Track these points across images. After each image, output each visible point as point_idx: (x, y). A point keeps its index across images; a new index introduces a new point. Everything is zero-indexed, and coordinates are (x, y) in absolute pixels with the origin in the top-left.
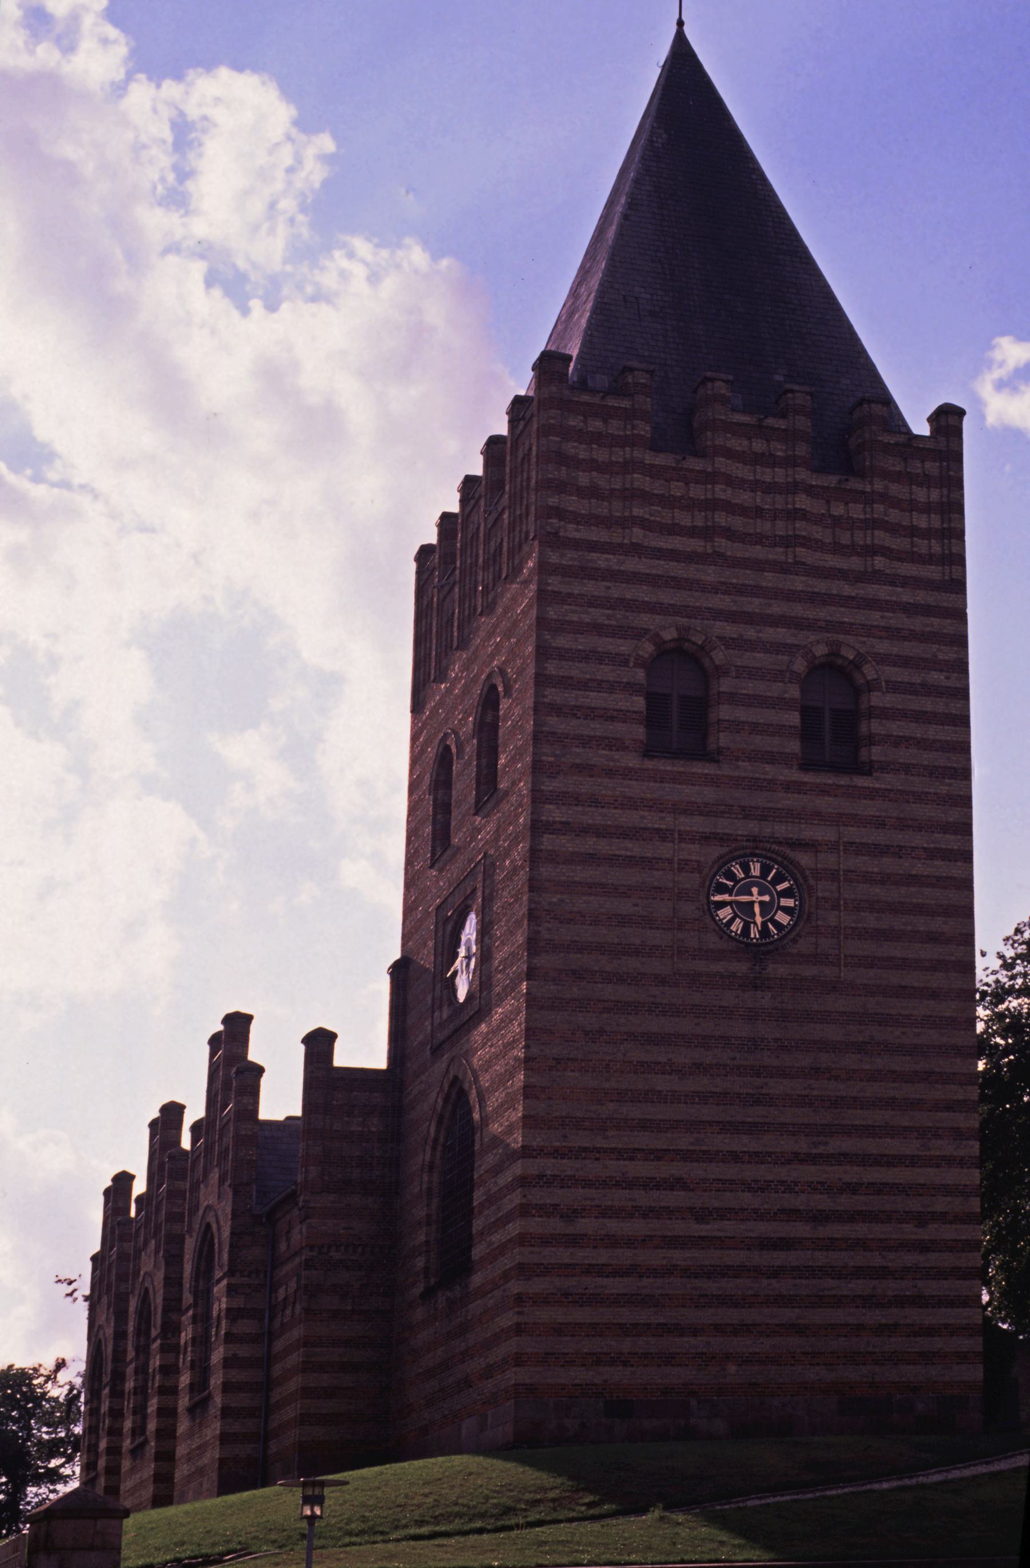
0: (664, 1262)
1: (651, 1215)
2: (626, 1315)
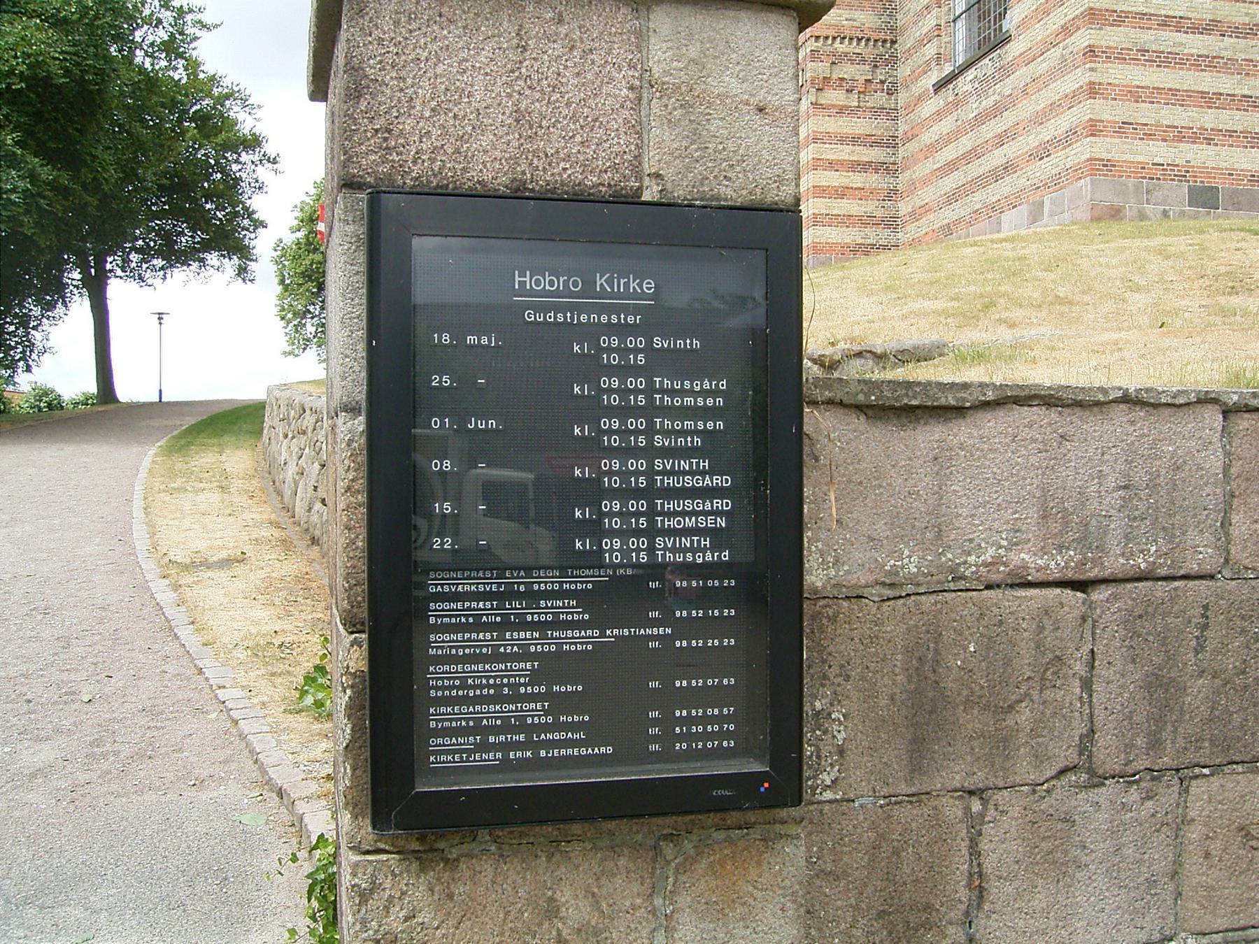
0: (1247, 20)
1: (321, 227)
2: (1208, 82)
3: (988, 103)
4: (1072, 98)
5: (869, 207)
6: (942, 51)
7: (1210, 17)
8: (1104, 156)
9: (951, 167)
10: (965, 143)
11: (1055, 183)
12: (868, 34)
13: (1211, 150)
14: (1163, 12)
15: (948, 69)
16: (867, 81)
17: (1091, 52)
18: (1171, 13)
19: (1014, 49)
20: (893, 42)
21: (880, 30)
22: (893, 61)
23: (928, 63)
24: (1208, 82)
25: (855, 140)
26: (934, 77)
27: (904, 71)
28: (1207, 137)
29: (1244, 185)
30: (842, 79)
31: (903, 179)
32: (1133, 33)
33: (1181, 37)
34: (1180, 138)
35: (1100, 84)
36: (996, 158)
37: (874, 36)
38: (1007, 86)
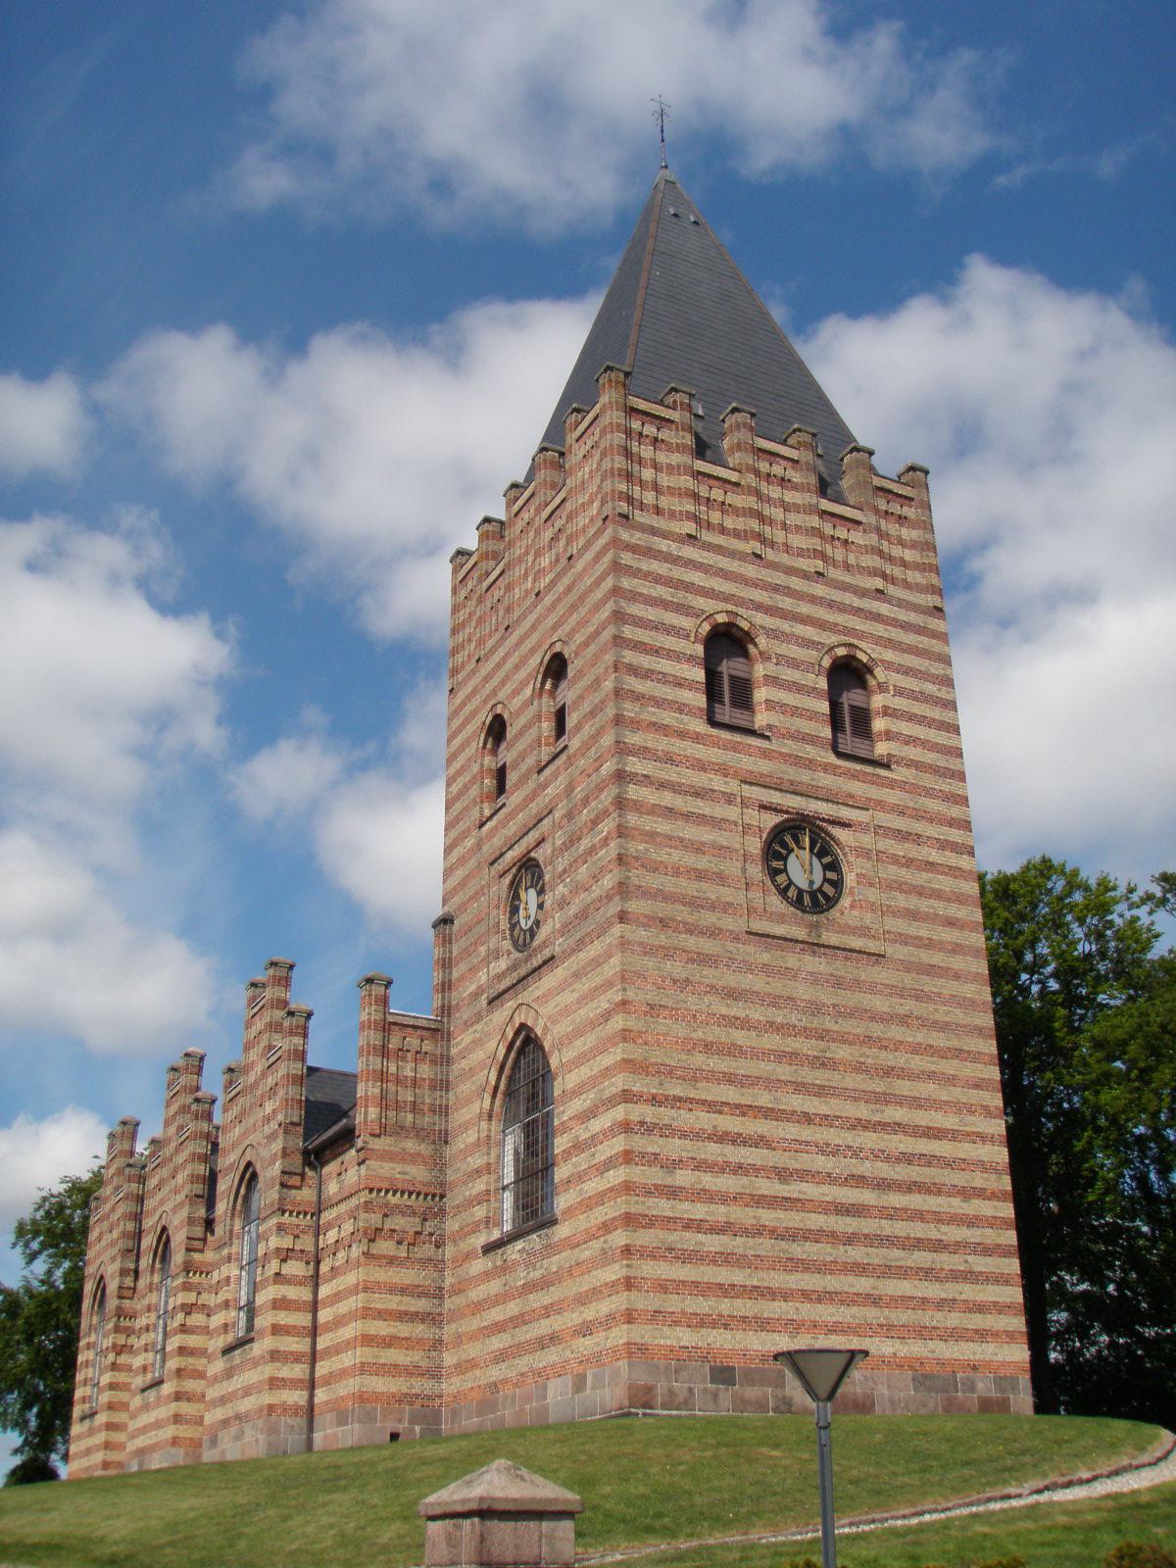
2: (725, 1275)
3: (536, 1274)
4: (612, 1287)
5: (415, 1357)
6: (491, 1215)
7: (724, 1219)
8: (639, 1340)
9: (498, 1328)
10: (513, 1308)
11: (596, 1359)
12: (419, 1187)
13: (728, 1335)
14: (686, 1216)
15: (496, 1235)
16: (416, 1233)
17: (627, 1251)
18: (692, 1217)
19: (562, 1231)
20: (442, 1196)
21: (430, 1183)
22: (441, 1213)
23: (477, 1224)
24: (725, 1275)
25: (404, 1290)
26: (481, 1239)
27: (452, 1225)
28: (724, 1323)
29: (756, 1364)
30: (393, 1231)
31: (448, 1331)
32: (661, 1234)
33: (700, 1237)
34: (702, 1324)
35: (635, 1278)
36: (543, 1327)
37: (424, 1190)
38: (554, 1263)
